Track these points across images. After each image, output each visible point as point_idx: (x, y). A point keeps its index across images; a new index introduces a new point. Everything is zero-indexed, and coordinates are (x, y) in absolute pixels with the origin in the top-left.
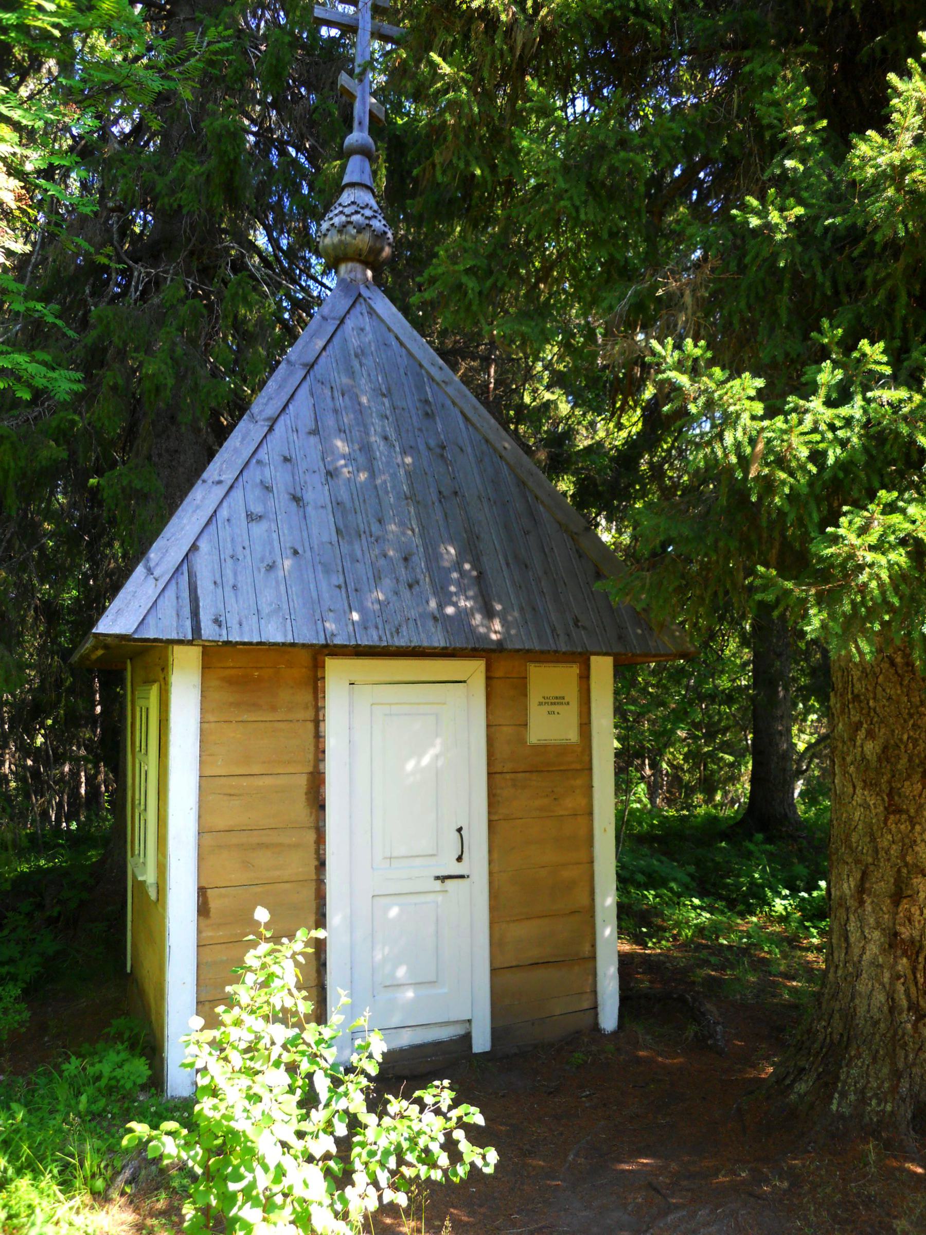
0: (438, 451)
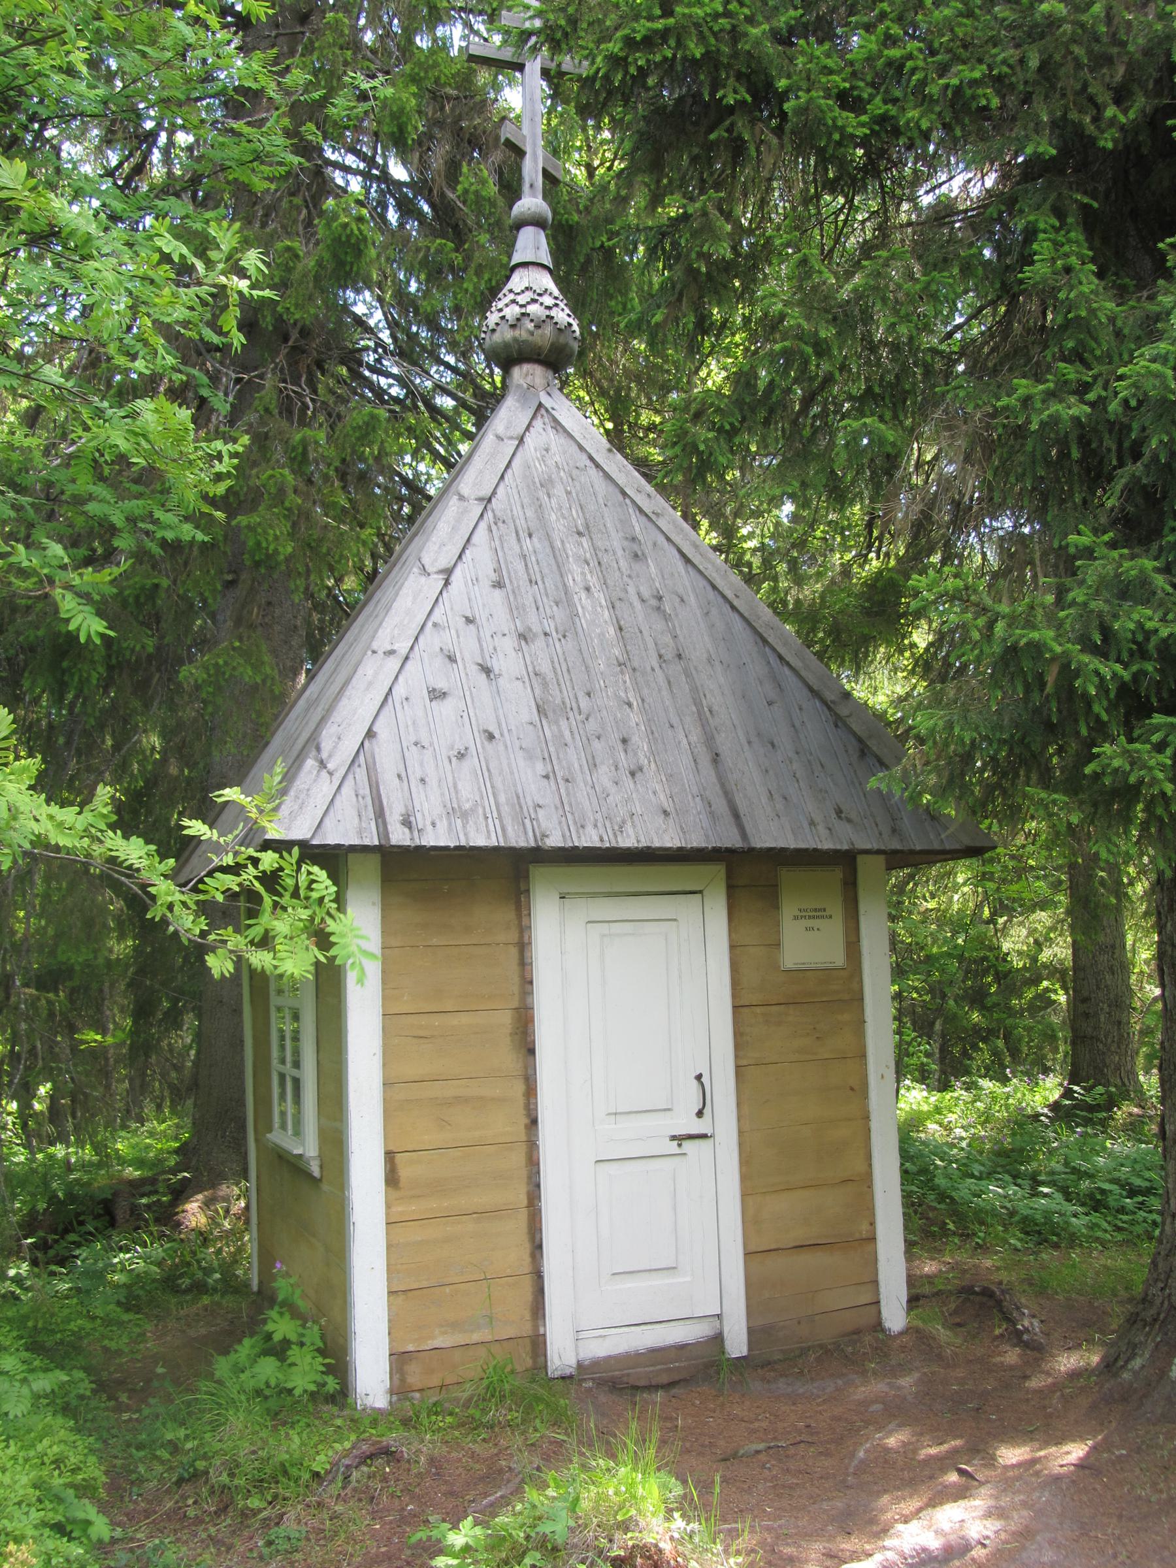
0: (654, 602)
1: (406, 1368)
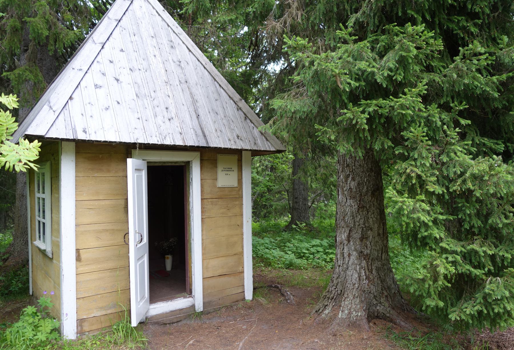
0: (178, 63)
1: (83, 324)
